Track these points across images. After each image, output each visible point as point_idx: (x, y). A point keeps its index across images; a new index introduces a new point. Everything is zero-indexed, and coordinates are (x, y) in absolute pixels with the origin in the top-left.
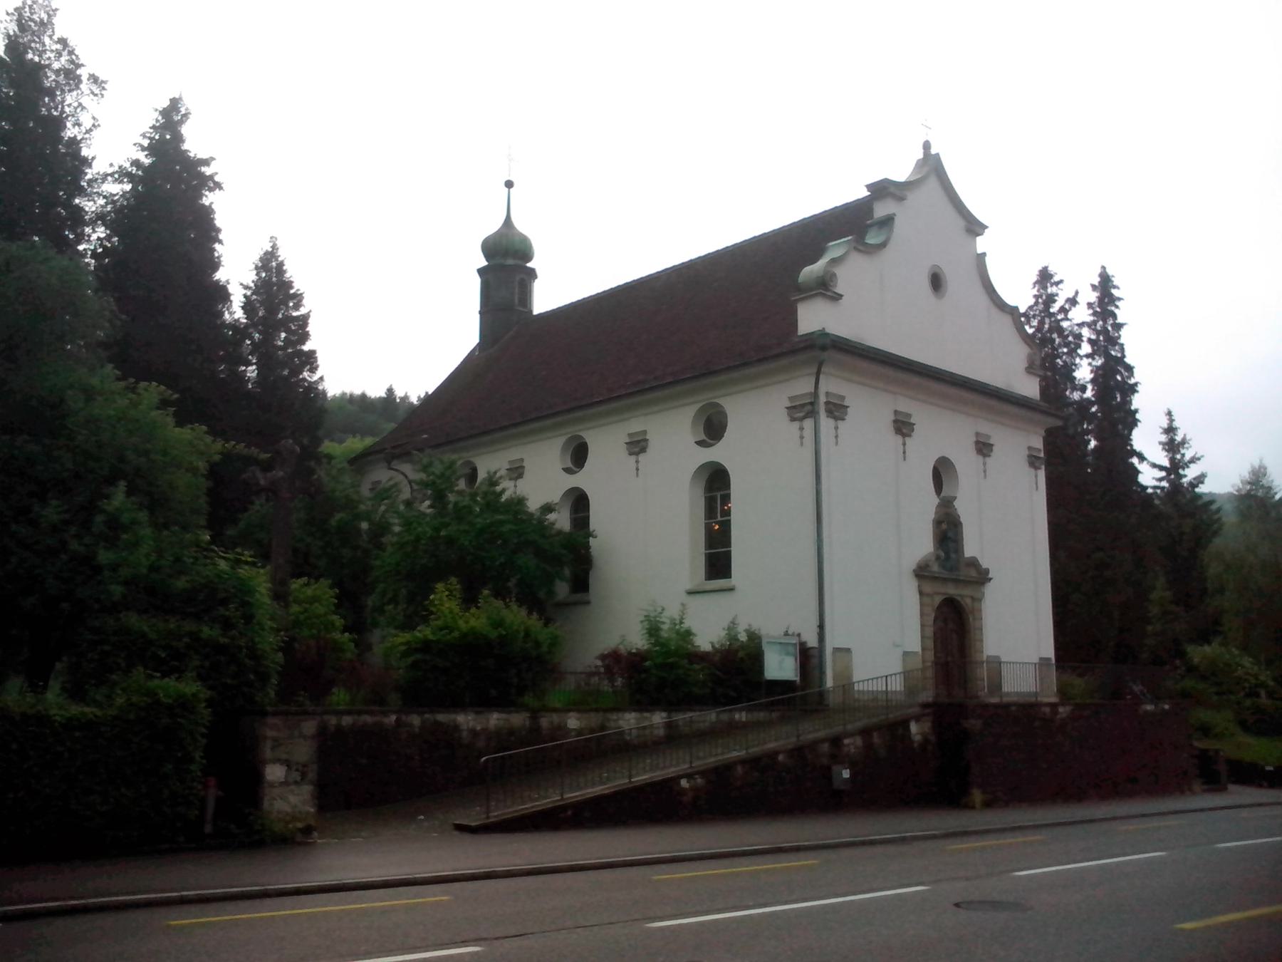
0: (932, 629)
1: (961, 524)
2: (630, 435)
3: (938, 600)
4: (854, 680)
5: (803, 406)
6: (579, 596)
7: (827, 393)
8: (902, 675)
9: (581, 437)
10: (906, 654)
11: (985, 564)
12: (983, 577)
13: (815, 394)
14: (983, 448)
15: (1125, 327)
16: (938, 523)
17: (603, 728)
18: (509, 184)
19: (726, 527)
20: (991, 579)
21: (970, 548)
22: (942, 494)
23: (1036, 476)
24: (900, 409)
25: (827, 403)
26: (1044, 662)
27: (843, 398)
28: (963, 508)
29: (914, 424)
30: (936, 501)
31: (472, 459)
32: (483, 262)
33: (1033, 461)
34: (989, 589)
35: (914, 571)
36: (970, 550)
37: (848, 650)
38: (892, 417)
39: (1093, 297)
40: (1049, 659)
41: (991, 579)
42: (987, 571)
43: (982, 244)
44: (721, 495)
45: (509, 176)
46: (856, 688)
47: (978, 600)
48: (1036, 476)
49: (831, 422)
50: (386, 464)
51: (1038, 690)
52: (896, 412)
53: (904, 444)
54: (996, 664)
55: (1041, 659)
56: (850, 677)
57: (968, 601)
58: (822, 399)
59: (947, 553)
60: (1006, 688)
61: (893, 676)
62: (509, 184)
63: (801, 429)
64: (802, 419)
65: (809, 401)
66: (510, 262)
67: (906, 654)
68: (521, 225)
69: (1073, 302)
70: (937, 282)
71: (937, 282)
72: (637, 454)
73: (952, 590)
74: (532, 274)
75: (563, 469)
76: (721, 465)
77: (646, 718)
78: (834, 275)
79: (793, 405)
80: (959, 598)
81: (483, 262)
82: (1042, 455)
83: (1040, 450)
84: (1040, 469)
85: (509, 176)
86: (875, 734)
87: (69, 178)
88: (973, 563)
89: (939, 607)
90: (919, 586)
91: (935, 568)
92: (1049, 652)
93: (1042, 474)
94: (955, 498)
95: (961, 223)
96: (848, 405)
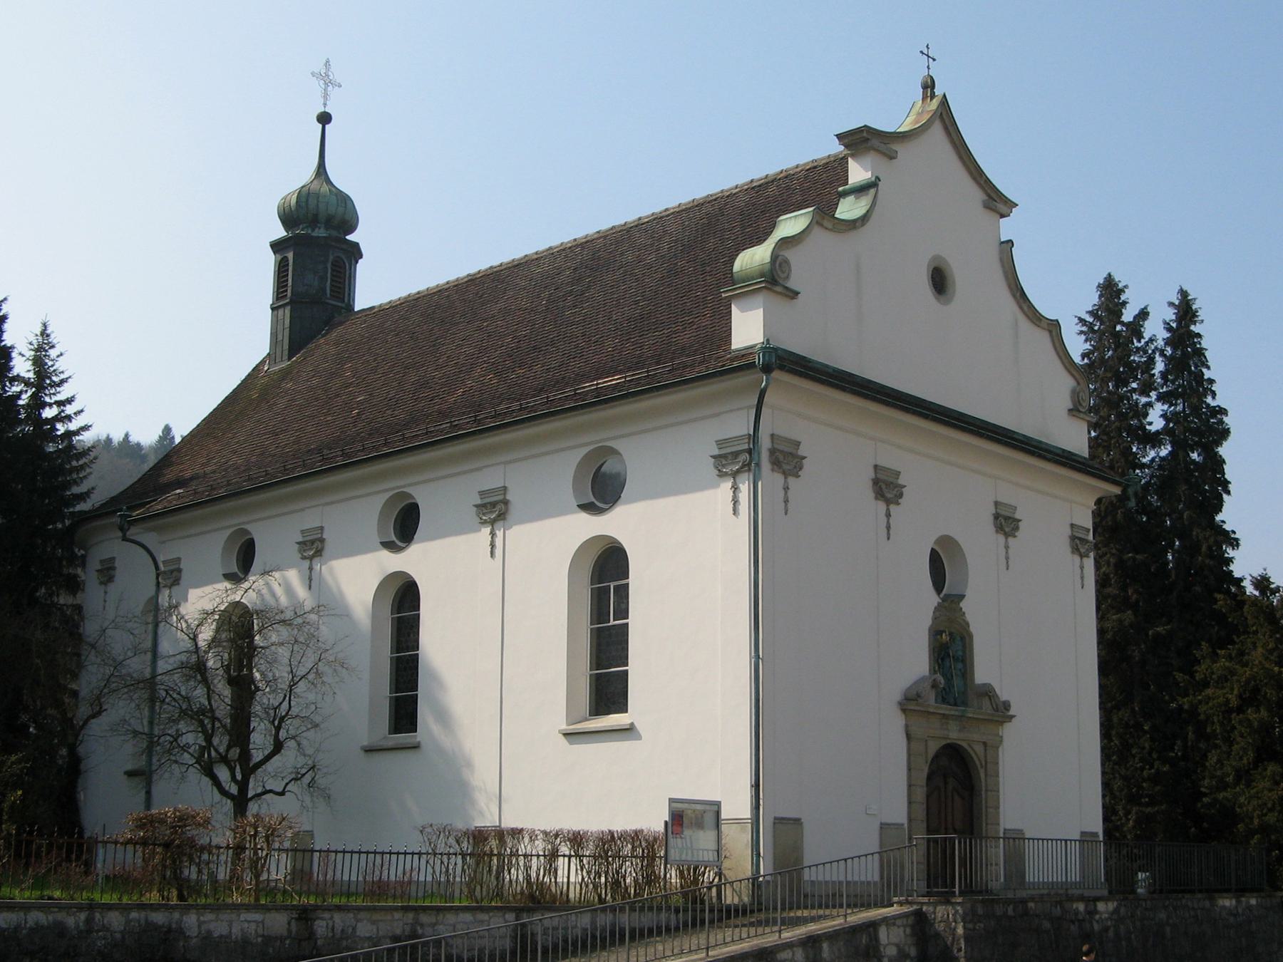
0: (925, 789)
1: (971, 636)
2: (482, 494)
3: (934, 747)
4: (806, 863)
5: (736, 455)
6: (403, 738)
7: (772, 436)
8: (876, 857)
9: (410, 496)
10: (883, 826)
11: (1003, 695)
12: (1001, 712)
13: (754, 437)
14: (1006, 523)
15: (836, 134)
16: (935, 633)
17: (414, 935)
18: (325, 119)
19: (621, 635)
20: (1013, 717)
21: (984, 671)
22: (945, 591)
23: (1082, 568)
24: (883, 462)
25: (772, 452)
26: (1086, 839)
27: (798, 444)
28: (975, 611)
29: (804, 458)
30: (933, 599)
31: (248, 527)
32: (280, 232)
33: (1077, 544)
34: (1008, 731)
35: (900, 703)
36: (982, 675)
37: (797, 821)
38: (1068, 531)
39: (1170, 315)
40: (1096, 834)
41: (1013, 717)
42: (1007, 705)
43: (1007, 228)
44: (614, 586)
45: (325, 105)
46: (806, 877)
47: (992, 747)
48: (1082, 568)
49: (779, 478)
50: (120, 534)
51: (1078, 880)
52: (1072, 526)
53: (888, 515)
54: (1016, 839)
55: (1083, 833)
56: (799, 859)
57: (979, 749)
58: (765, 443)
59: (949, 679)
60: (1030, 877)
61: (856, 860)
62: (325, 119)
63: (735, 489)
64: (735, 475)
65: (746, 447)
66: (320, 232)
67: (883, 826)
68: (340, 178)
69: (1143, 314)
70: (940, 281)
71: (940, 281)
72: (493, 522)
73: (954, 734)
74: (355, 252)
75: (381, 543)
76: (613, 538)
77: (482, 922)
78: (786, 262)
79: (723, 452)
80: (965, 745)
81: (280, 232)
82: (1091, 537)
83: (1088, 530)
84: (1087, 556)
85: (325, 105)
86: (825, 946)
87: (1163, 543)
88: (987, 692)
89: (937, 756)
90: (907, 726)
91: (931, 697)
92: (1095, 824)
93: (1089, 563)
94: (962, 597)
95: (978, 195)
96: (804, 455)
